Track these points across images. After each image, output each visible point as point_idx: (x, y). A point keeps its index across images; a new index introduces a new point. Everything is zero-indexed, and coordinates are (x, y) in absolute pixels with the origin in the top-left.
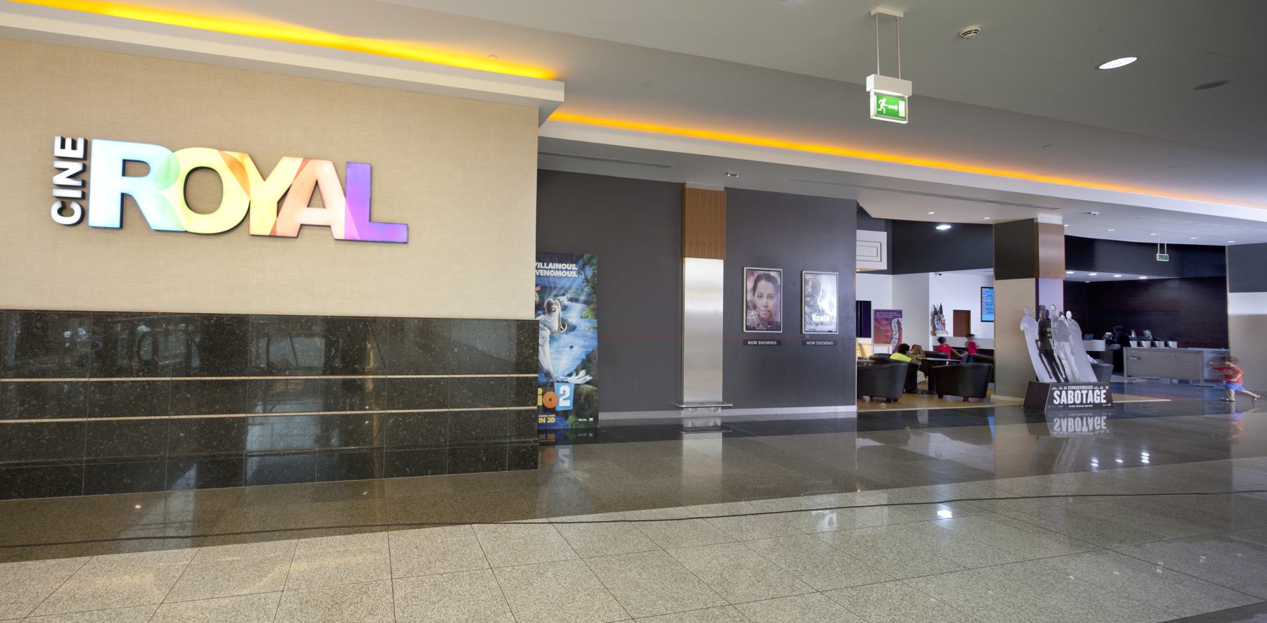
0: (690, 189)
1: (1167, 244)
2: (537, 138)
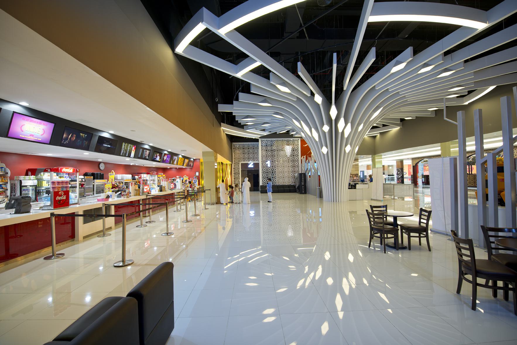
2: (506, 205)
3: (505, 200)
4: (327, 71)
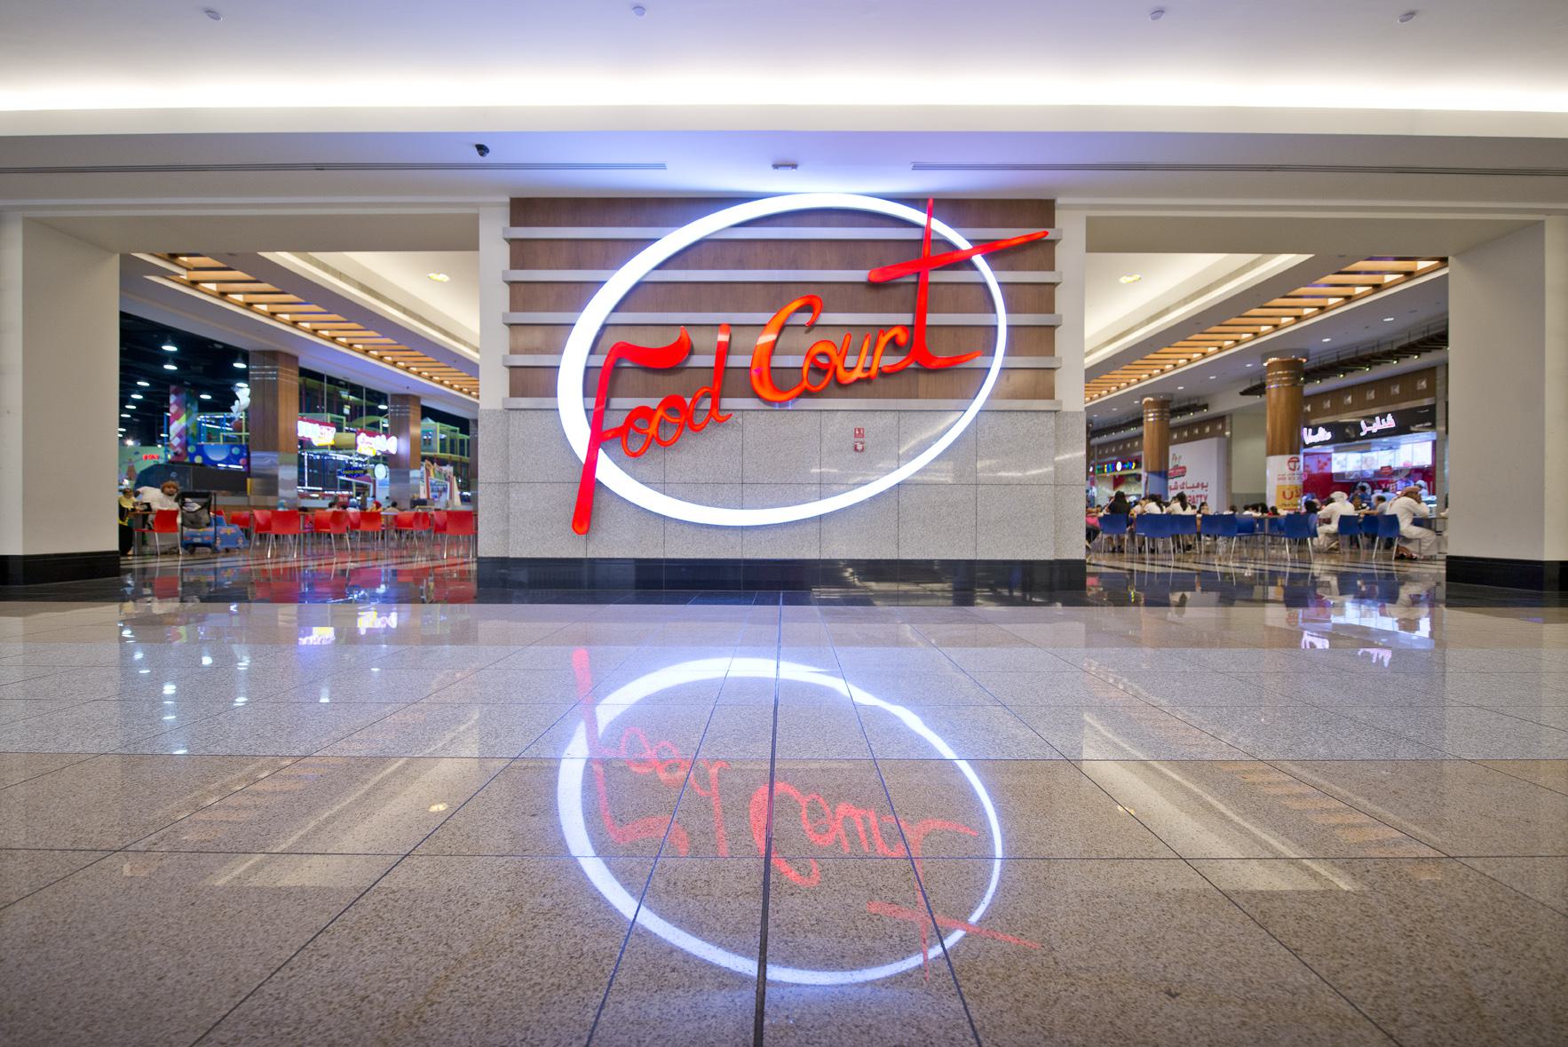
0: (752, 958)
3: (958, 233)
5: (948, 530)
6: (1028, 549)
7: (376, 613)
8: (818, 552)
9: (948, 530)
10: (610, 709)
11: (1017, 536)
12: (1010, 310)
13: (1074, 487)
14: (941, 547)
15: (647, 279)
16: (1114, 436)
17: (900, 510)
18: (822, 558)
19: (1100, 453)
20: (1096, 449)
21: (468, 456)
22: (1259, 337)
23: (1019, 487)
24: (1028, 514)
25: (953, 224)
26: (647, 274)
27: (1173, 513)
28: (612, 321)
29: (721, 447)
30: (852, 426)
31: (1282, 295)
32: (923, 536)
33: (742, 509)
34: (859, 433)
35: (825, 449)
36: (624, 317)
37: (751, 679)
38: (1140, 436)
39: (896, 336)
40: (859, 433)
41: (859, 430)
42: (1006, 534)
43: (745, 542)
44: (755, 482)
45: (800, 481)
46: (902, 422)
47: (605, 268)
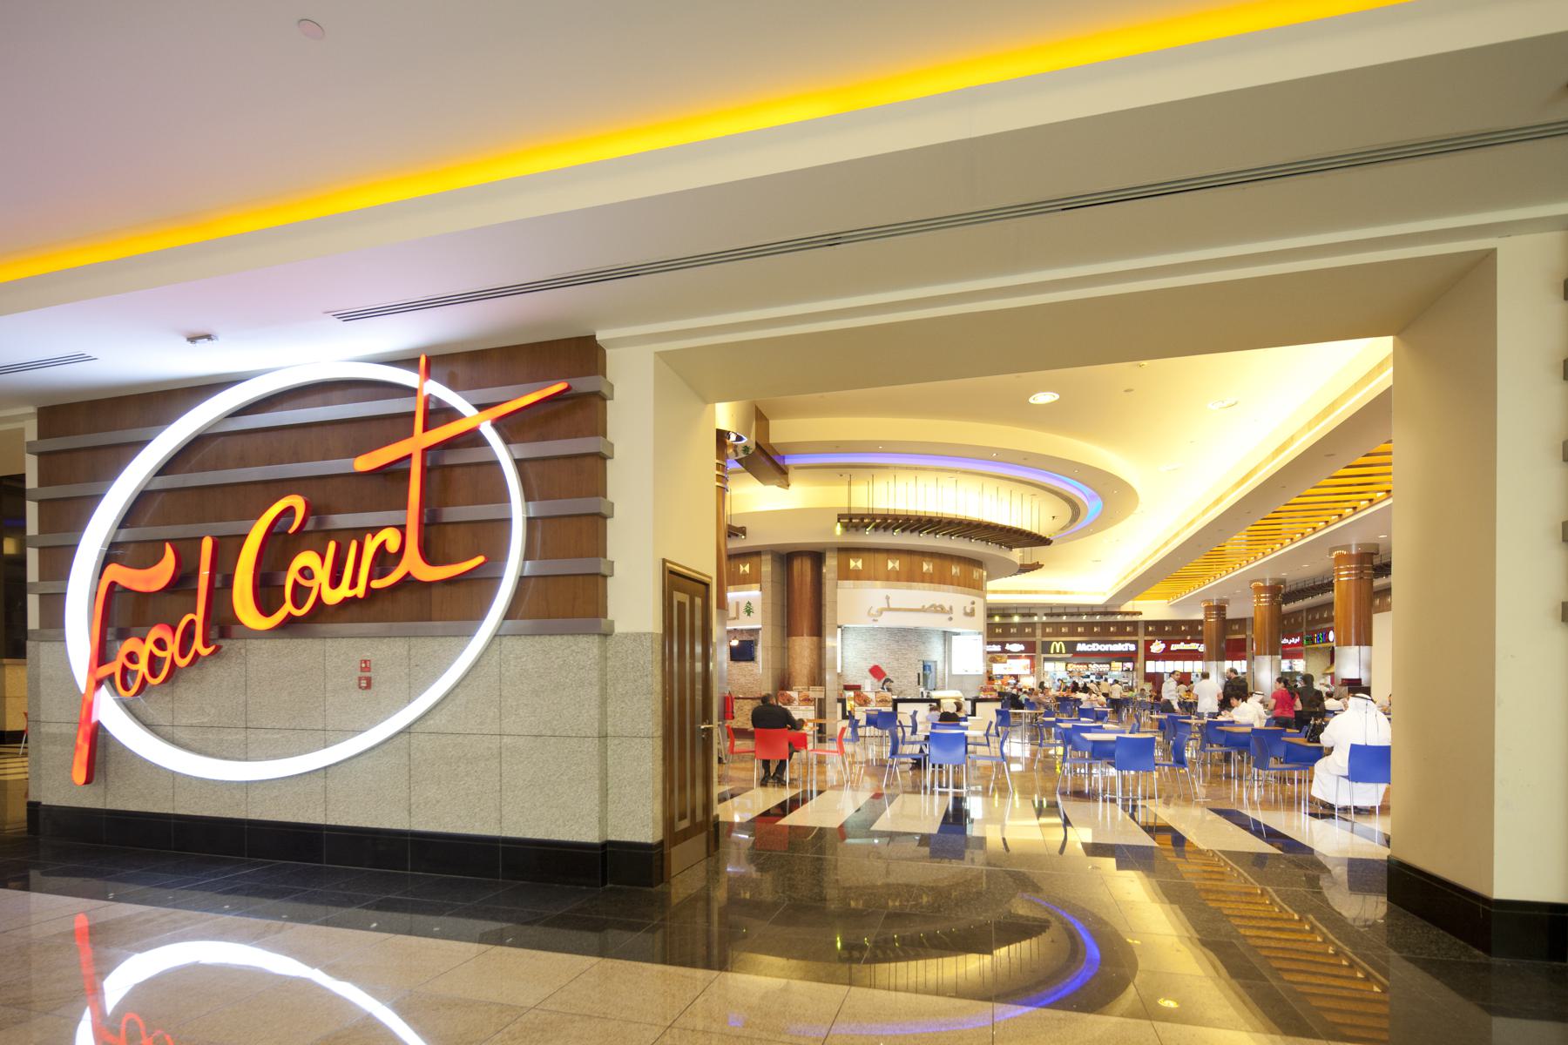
1: (988, 637)
4: (820, 735)
5: (467, 795)
6: (565, 825)
7: (805, 728)
8: (323, 815)
9: (467, 795)
10: (118, 984)
11: (552, 807)
12: (528, 496)
13: (638, 740)
14: (459, 817)
15: (152, 487)
16: (1309, 602)
17: (412, 767)
18: (328, 823)
19: (1310, 617)
20: (1305, 614)
21: (1328, 586)
22: (1344, 519)
23: (553, 739)
24: (565, 778)
25: (453, 384)
26: (149, 483)
27: (1222, 697)
28: (120, 539)
29: (225, 683)
30: (358, 658)
31: (1327, 476)
32: (438, 802)
33: (246, 760)
34: (366, 666)
35: (329, 687)
36: (124, 535)
37: (121, 1001)
38: (1329, 605)
39: (383, 545)
40: (366, 666)
41: (365, 662)
42: (538, 804)
43: (249, 799)
44: (259, 726)
45: (303, 726)
46: (413, 652)
47: (95, 480)
